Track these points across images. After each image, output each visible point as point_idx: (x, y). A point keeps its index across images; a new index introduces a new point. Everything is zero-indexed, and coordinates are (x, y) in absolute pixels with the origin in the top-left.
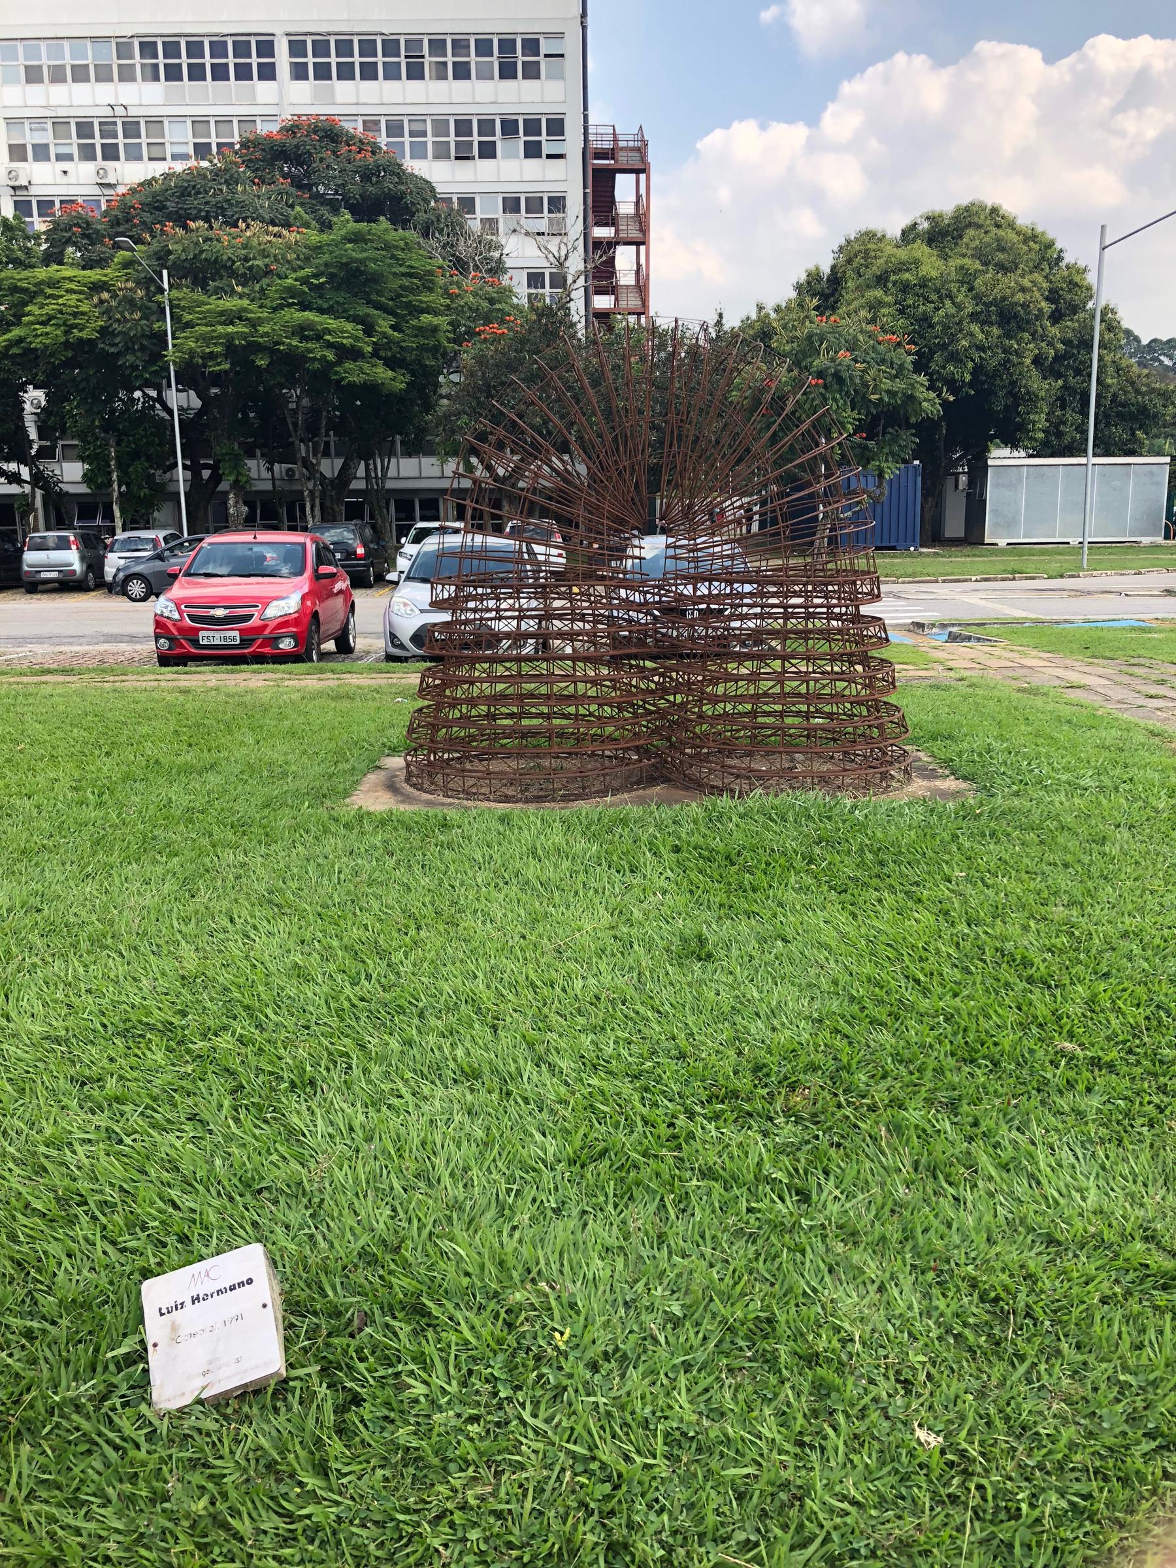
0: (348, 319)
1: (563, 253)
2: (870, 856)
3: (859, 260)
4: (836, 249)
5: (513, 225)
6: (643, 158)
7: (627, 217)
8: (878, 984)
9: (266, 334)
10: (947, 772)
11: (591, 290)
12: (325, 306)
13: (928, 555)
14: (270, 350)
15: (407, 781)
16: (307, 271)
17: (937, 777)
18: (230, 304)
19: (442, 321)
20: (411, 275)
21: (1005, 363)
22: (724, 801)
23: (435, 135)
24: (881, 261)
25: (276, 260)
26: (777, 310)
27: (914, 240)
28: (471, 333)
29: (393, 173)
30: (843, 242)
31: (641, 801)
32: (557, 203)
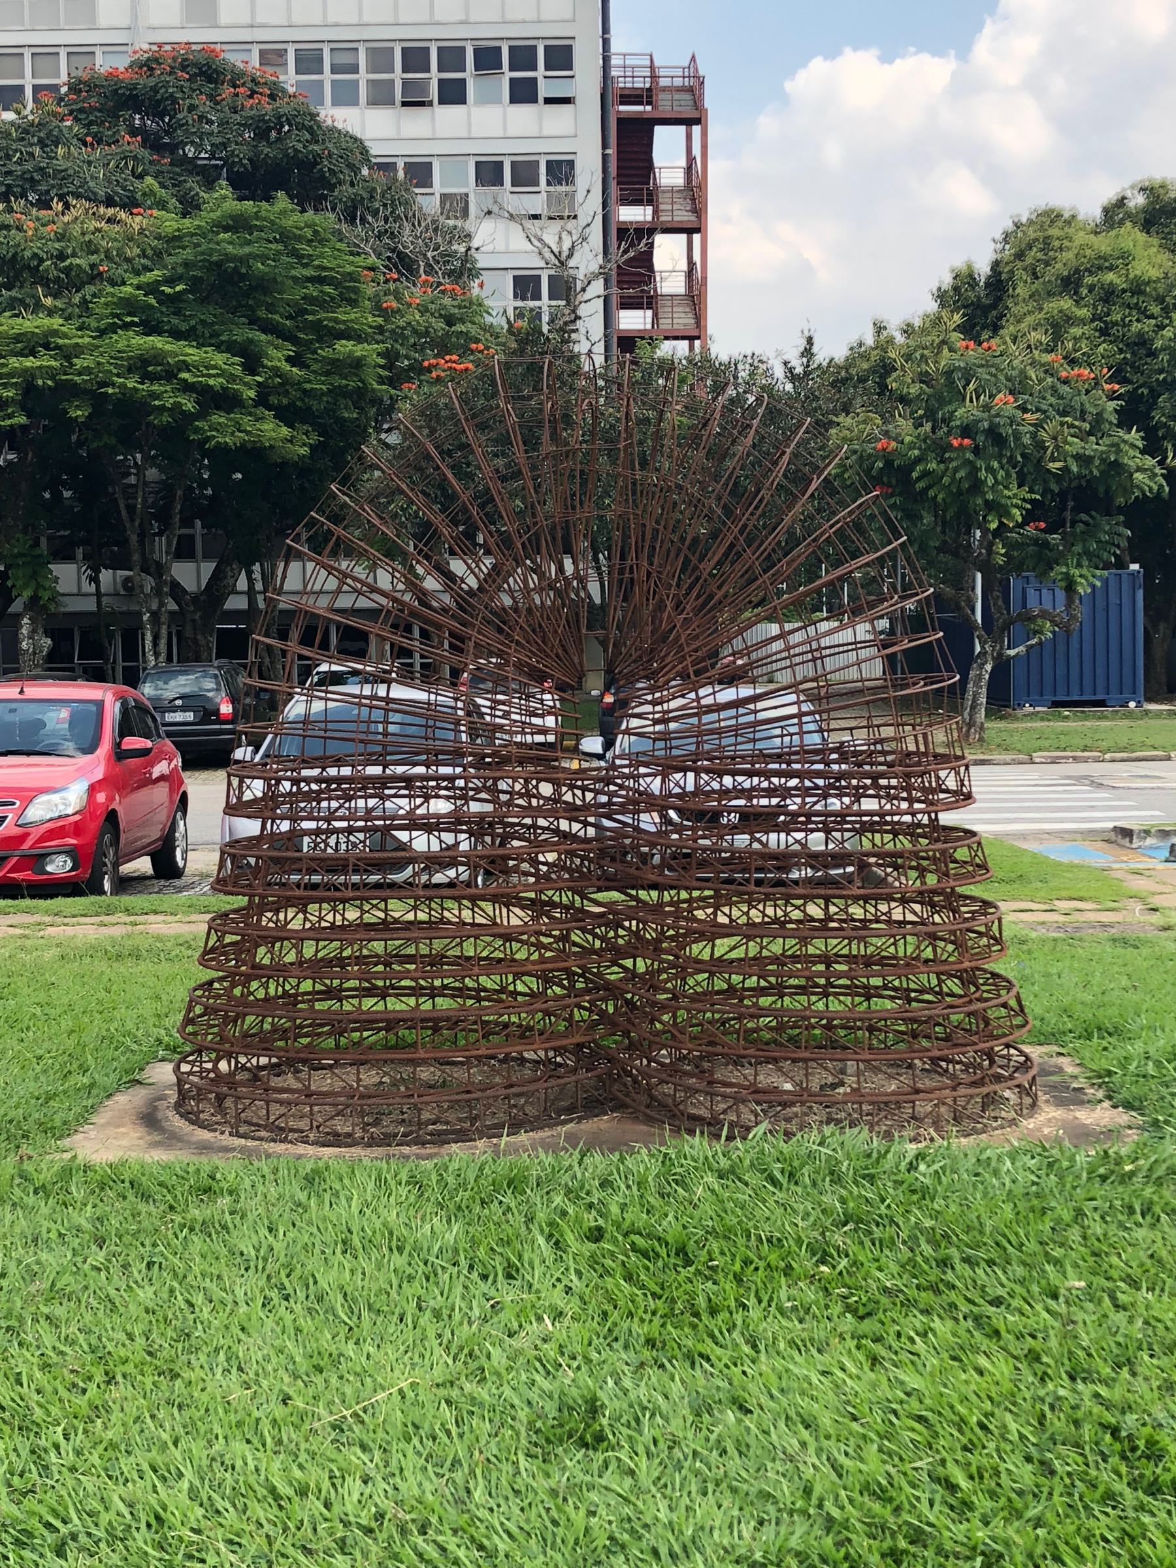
0: (219, 347)
1: (567, 245)
2: (927, 1250)
3: (1033, 254)
4: (999, 236)
6: (698, 104)
7: (672, 190)
8: (881, 1495)
9: (87, 370)
10: (1100, 1094)
11: (614, 301)
12: (184, 327)
13: (1159, 715)
14: (94, 396)
15: (178, 1106)
16: (157, 274)
17: (1081, 1103)
18: (30, 323)
19: (368, 351)
20: (320, 280)
22: (697, 1145)
23: (372, 69)
24: (1069, 256)
25: (108, 256)
26: (908, 330)
27: (1121, 223)
28: (418, 370)
29: (301, 127)
30: (1010, 226)
31: (551, 1147)
32: (561, 171)
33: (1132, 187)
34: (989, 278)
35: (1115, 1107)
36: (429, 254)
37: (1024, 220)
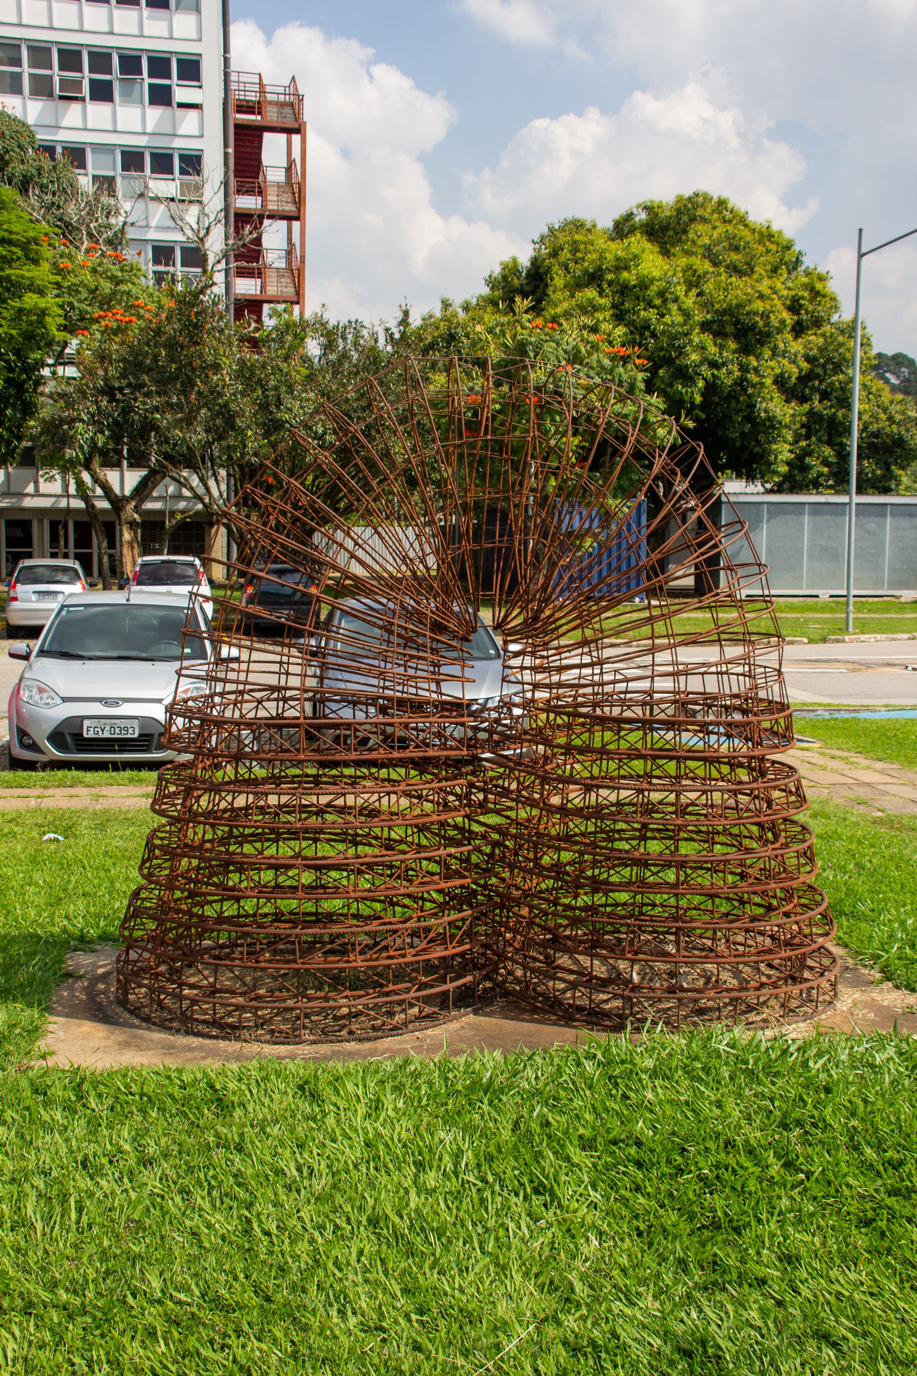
4: (536, 239)
5: (138, 187)
6: (297, 115)
7: (279, 185)
11: (232, 272)
19: (49, 302)
21: (741, 382)
26: (466, 308)
33: (638, 206)
34: (529, 271)
35: (897, 987)
36: (92, 226)
37: (557, 227)
